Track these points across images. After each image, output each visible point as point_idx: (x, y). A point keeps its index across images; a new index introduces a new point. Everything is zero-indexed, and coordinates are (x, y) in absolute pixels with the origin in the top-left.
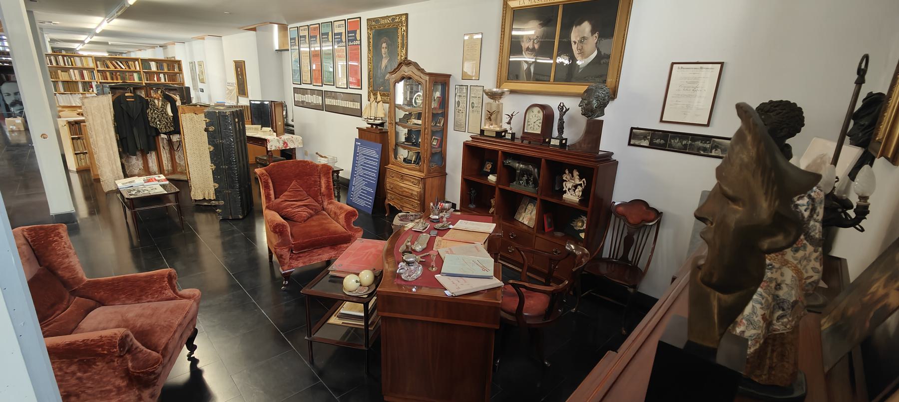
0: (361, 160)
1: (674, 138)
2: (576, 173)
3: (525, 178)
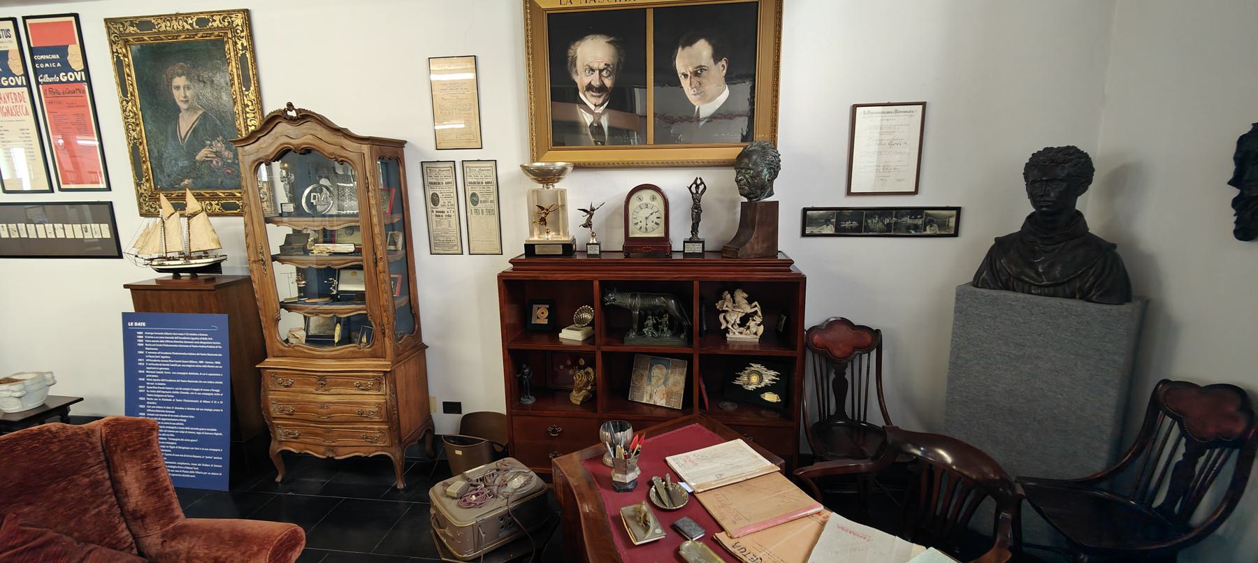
0: (155, 365)
1: (872, 217)
2: (741, 296)
3: (650, 322)
